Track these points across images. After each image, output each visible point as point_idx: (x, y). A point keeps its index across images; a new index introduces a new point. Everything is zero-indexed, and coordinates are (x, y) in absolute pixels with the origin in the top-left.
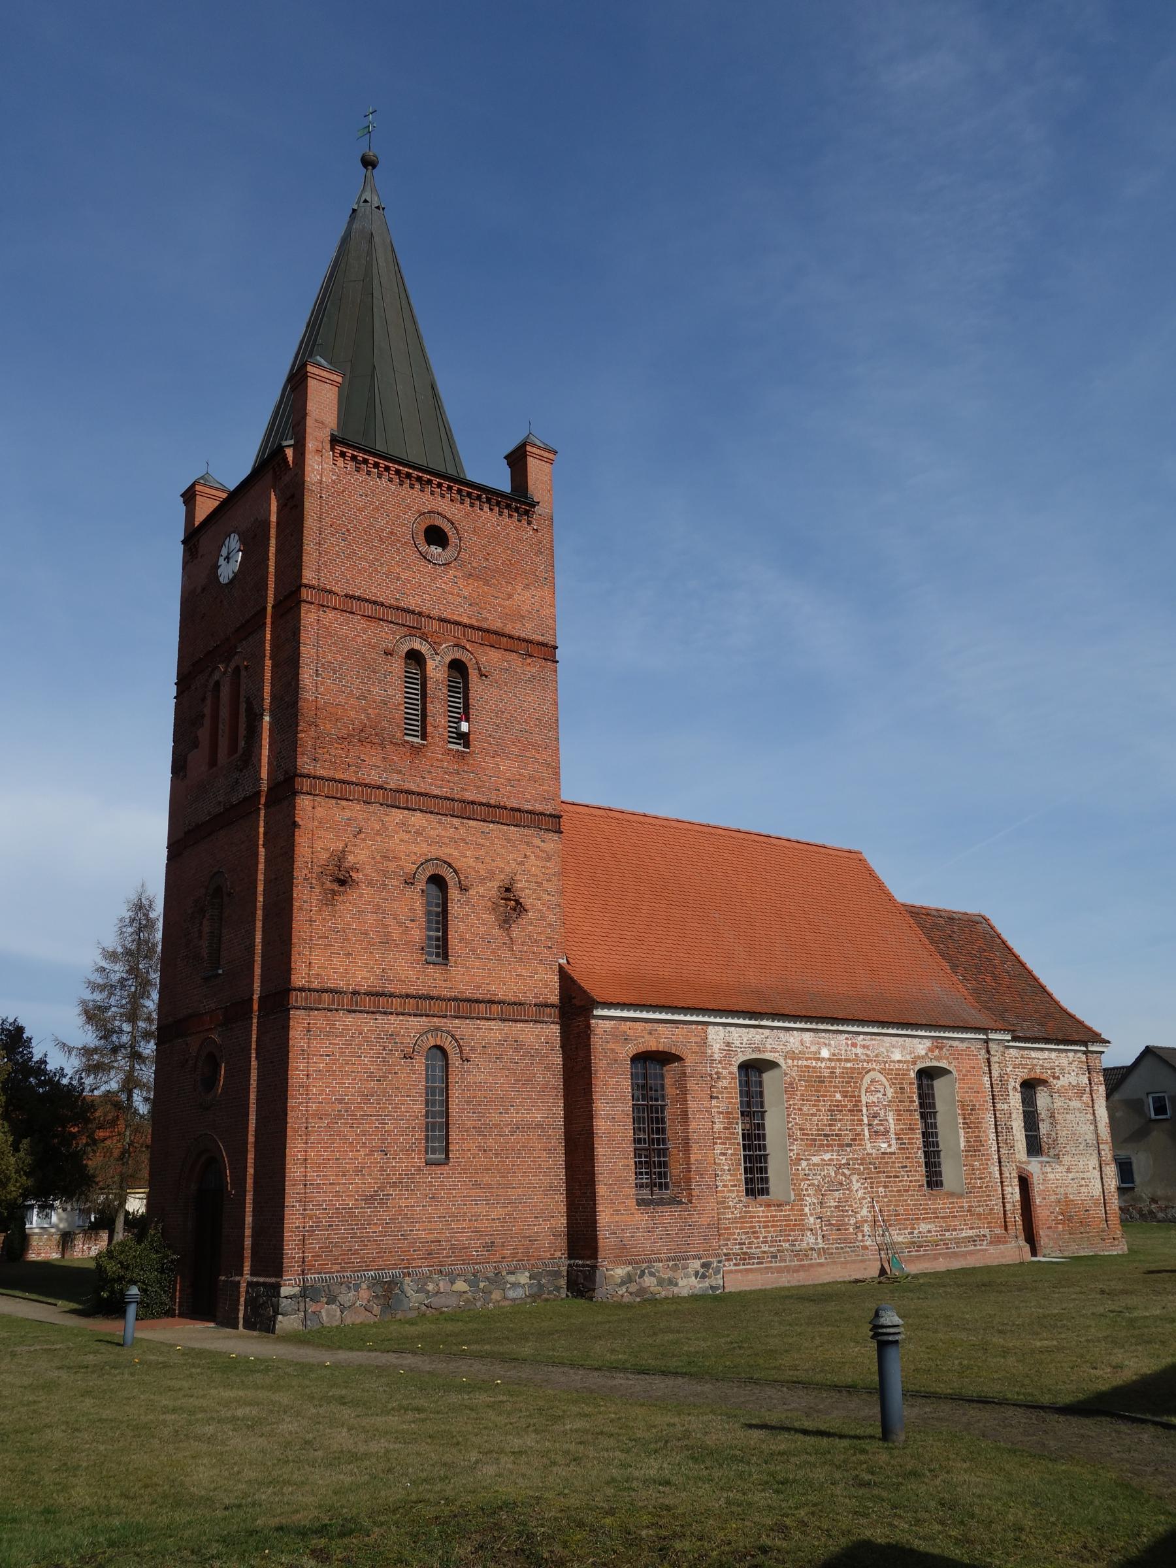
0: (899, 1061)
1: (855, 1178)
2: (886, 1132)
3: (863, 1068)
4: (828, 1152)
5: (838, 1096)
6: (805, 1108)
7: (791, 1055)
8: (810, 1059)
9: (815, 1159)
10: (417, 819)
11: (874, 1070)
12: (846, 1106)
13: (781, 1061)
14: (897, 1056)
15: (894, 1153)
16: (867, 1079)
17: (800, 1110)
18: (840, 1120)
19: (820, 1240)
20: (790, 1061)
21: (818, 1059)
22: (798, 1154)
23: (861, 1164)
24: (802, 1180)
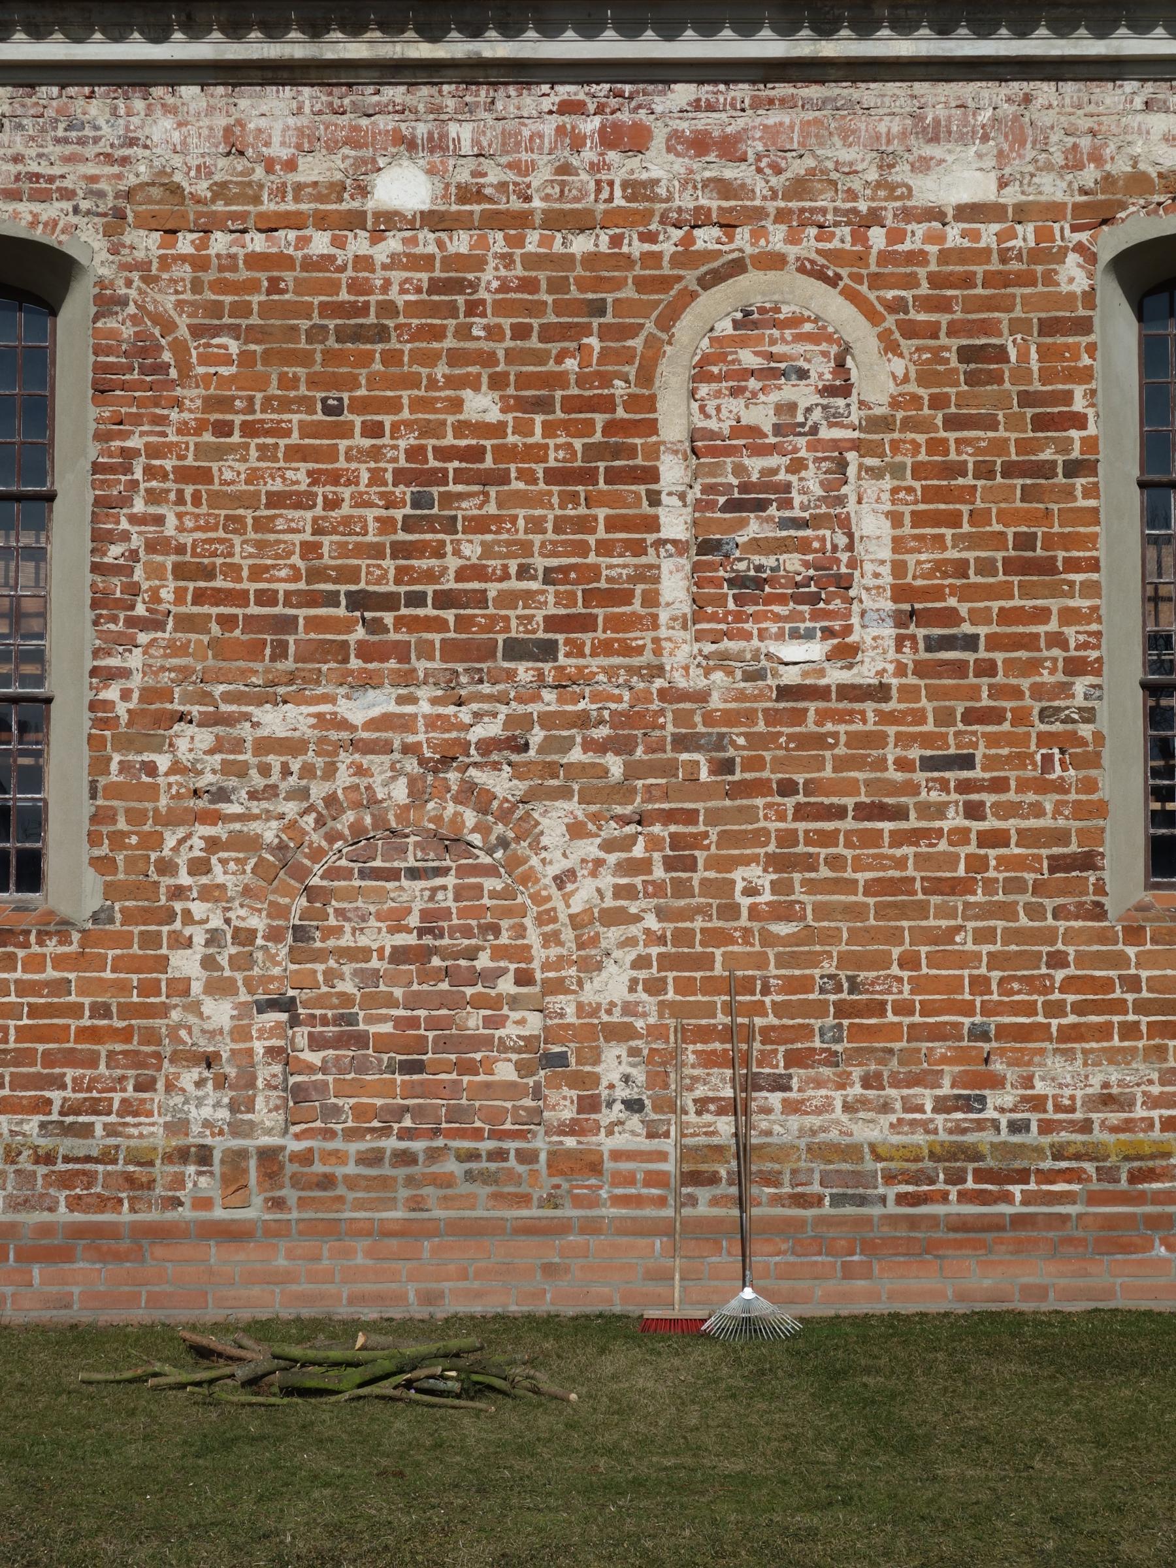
0: (971, 212)
1: (553, 820)
2: (832, 582)
3: (687, 257)
4: (368, 682)
5: (482, 405)
6: (229, 472)
7: (167, 208)
8: (294, 221)
9: (274, 720)
10: (395, 93)
11: (775, 261)
12: (536, 453)
13: (87, 244)
14: (961, 178)
15: (880, 692)
16: (714, 311)
17: (204, 476)
18: (479, 525)
19: (265, 1112)
20: (147, 244)
21: (355, 221)
22: (148, 695)
23: (621, 746)
24: (171, 819)
